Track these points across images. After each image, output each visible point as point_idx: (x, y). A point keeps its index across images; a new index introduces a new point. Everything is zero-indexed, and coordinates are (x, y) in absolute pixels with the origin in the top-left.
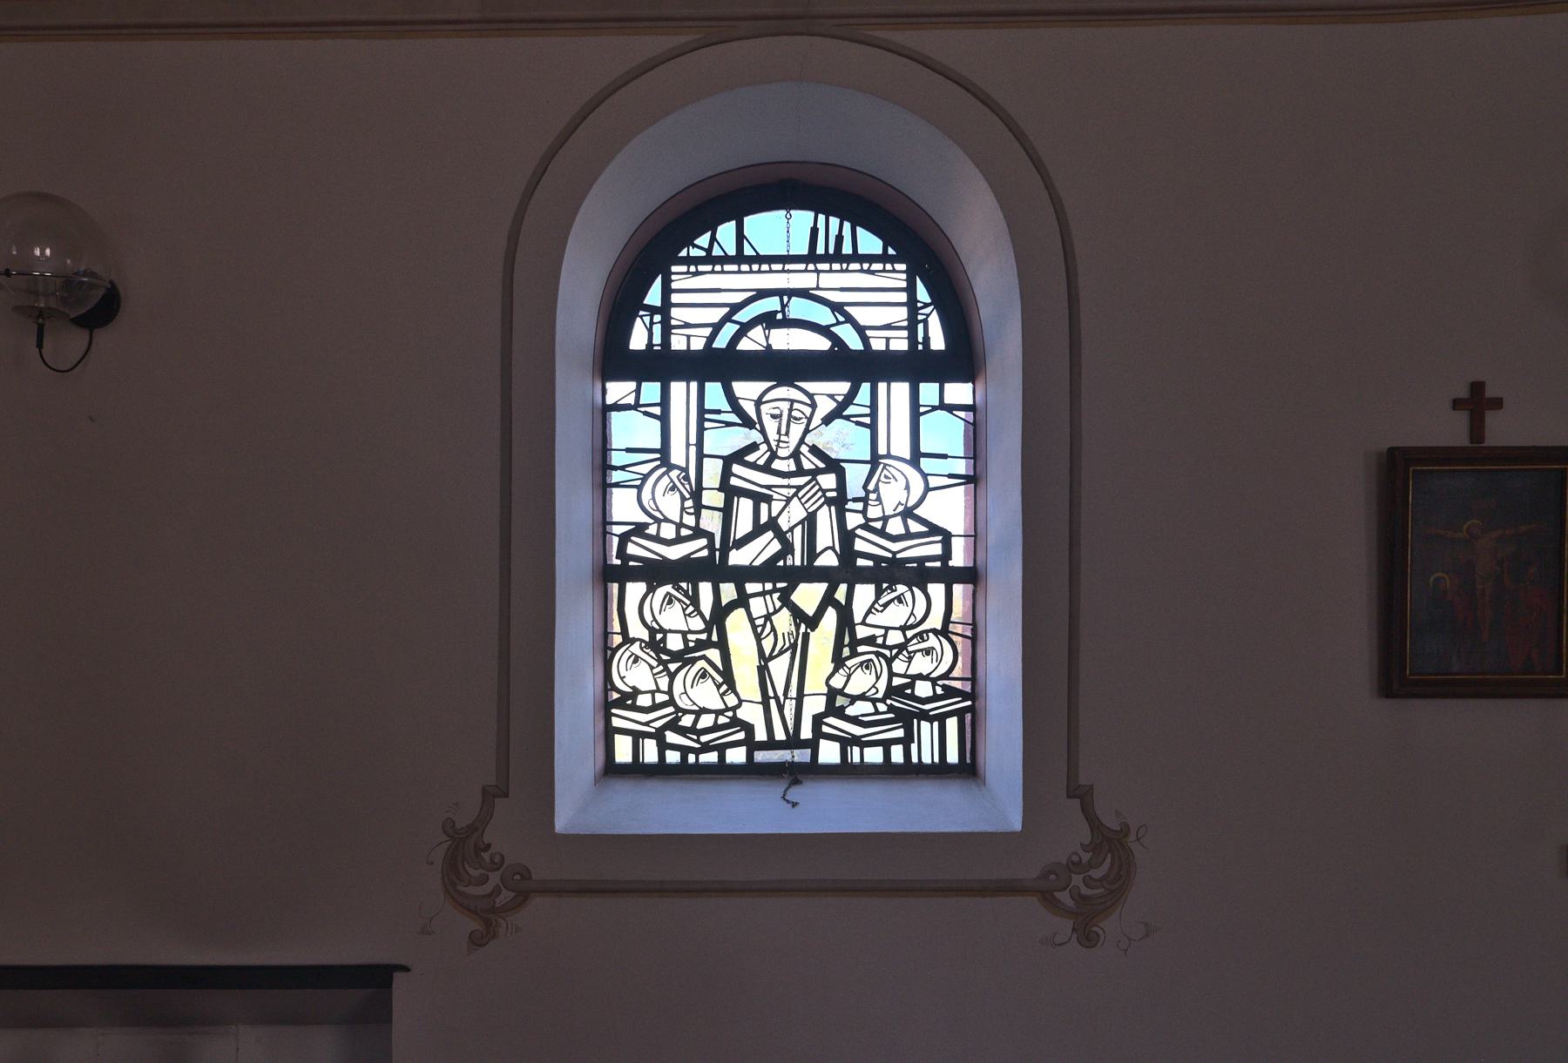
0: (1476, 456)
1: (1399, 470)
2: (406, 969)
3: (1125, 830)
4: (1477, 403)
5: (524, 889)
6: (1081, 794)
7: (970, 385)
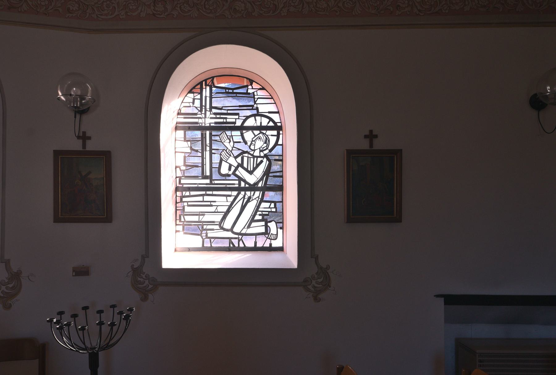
3: (328, 267)
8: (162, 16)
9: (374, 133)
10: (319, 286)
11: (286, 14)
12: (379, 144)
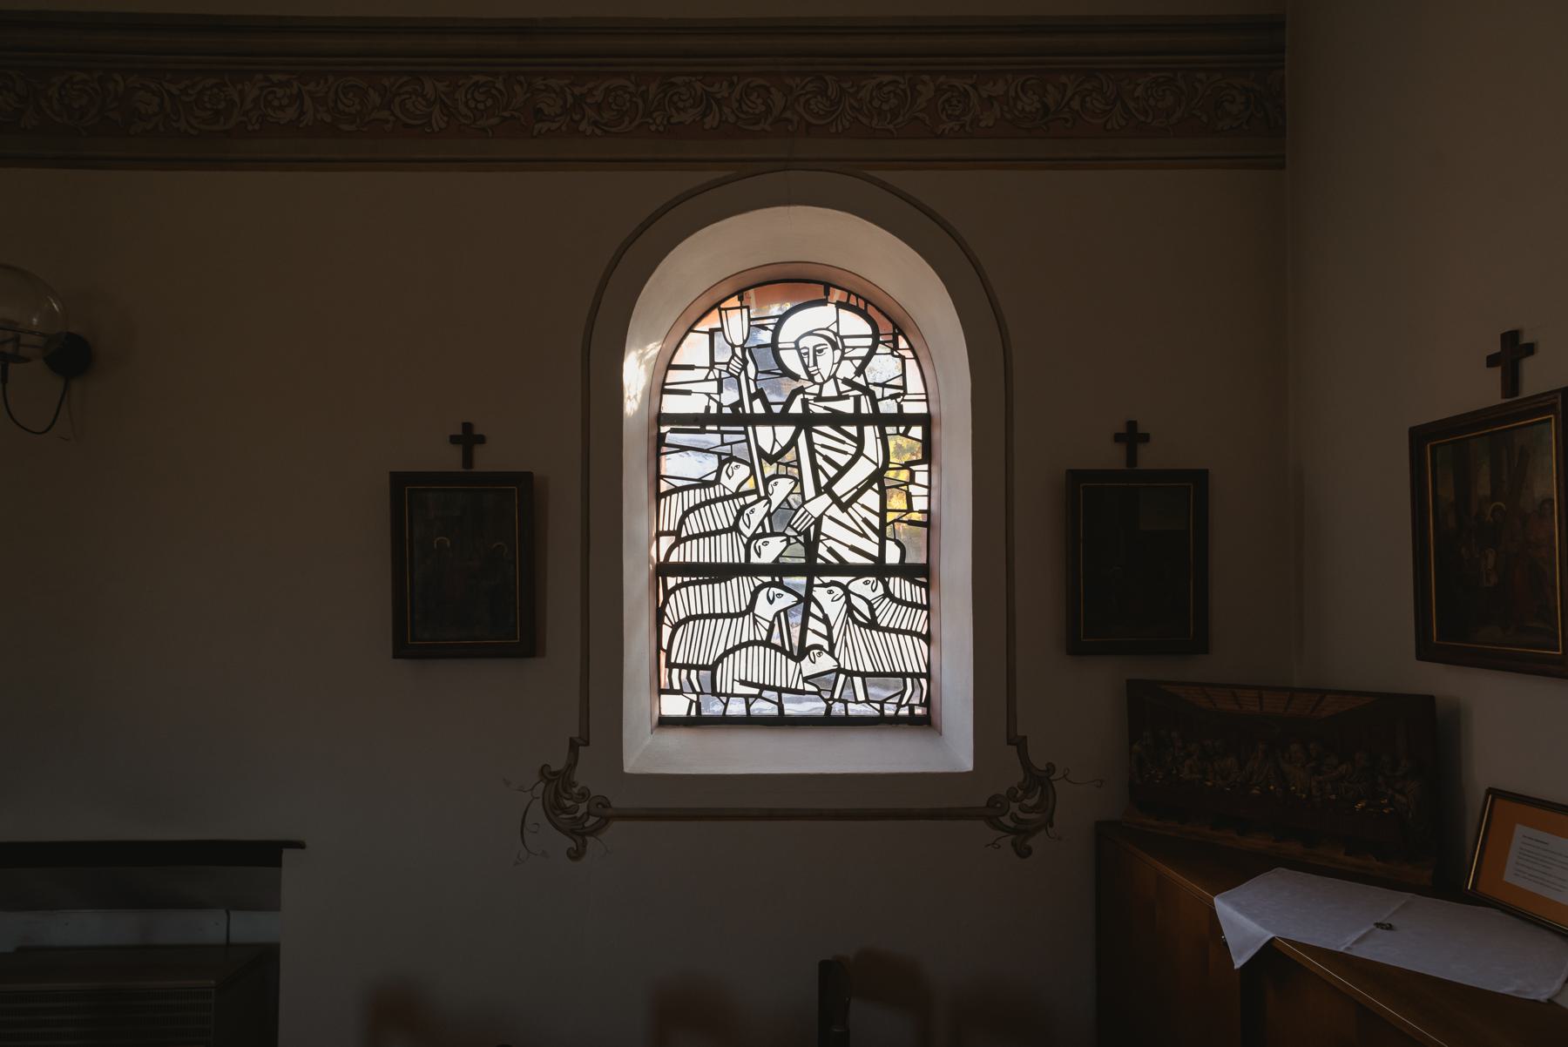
0: (1516, 410)
1: (407, 489)
2: (300, 845)
3: (1051, 768)
4: (468, 439)
5: (606, 815)
6: (1018, 743)
7: (664, 411)
8: (757, 128)
9: (477, 431)
10: (1033, 816)
11: (257, 127)
12: (487, 460)
